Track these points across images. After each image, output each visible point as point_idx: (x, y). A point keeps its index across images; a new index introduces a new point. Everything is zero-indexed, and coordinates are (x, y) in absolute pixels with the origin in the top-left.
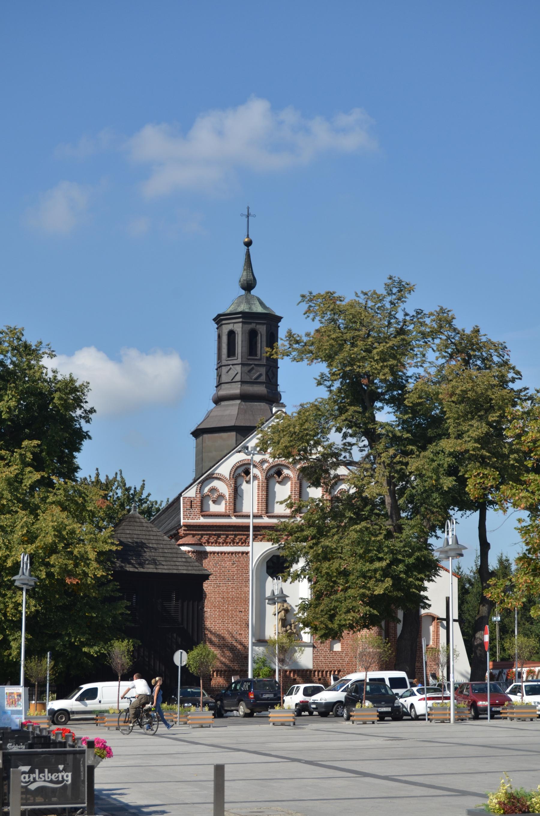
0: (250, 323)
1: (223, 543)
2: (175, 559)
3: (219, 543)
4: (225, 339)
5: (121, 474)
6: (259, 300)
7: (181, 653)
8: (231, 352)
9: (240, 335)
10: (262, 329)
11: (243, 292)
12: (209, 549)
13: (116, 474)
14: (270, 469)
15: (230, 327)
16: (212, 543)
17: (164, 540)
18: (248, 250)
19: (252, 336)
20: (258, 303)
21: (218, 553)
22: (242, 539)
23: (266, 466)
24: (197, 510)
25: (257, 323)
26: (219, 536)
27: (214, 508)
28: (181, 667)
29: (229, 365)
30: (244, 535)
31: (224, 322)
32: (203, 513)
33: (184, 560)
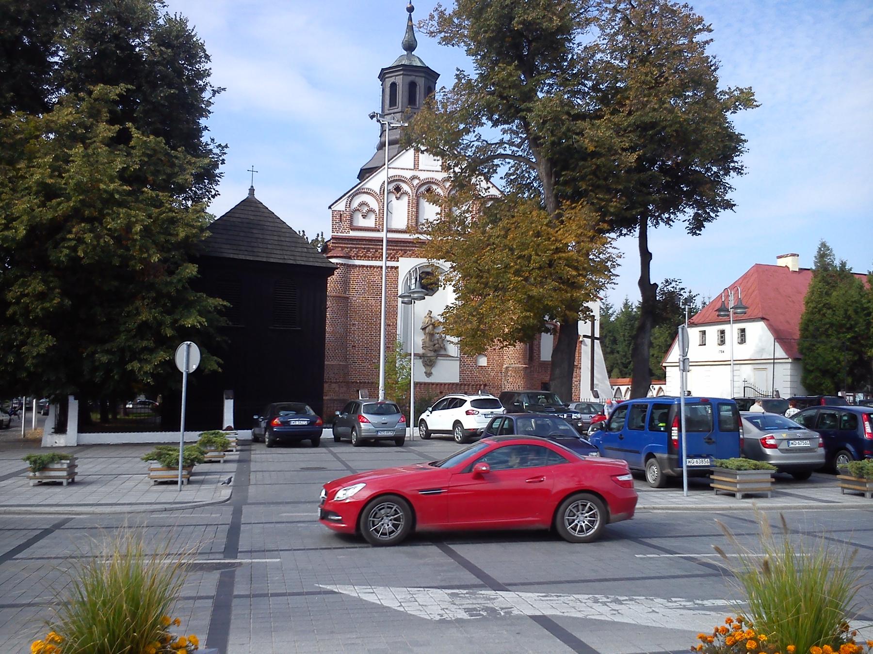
0: (410, 75)
1: (372, 258)
2: (293, 249)
3: (369, 257)
4: (388, 91)
5: (322, 235)
6: (419, 58)
7: (189, 346)
8: (393, 102)
9: (401, 86)
10: (421, 82)
11: (405, 53)
12: (358, 262)
13: (318, 234)
14: (420, 186)
15: (392, 80)
16: (361, 257)
17: (259, 212)
18: (410, 15)
19: (412, 86)
20: (418, 60)
21: (367, 267)
22: (391, 254)
23: (416, 182)
24: (346, 224)
25: (416, 76)
26: (368, 250)
27: (361, 222)
28: (189, 375)
29: (391, 114)
30: (393, 250)
31: (387, 76)
32: (351, 228)
33: (305, 250)
